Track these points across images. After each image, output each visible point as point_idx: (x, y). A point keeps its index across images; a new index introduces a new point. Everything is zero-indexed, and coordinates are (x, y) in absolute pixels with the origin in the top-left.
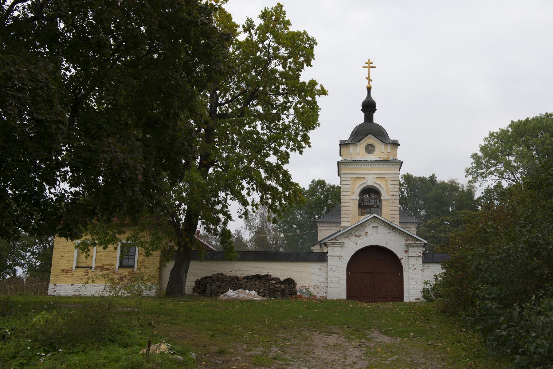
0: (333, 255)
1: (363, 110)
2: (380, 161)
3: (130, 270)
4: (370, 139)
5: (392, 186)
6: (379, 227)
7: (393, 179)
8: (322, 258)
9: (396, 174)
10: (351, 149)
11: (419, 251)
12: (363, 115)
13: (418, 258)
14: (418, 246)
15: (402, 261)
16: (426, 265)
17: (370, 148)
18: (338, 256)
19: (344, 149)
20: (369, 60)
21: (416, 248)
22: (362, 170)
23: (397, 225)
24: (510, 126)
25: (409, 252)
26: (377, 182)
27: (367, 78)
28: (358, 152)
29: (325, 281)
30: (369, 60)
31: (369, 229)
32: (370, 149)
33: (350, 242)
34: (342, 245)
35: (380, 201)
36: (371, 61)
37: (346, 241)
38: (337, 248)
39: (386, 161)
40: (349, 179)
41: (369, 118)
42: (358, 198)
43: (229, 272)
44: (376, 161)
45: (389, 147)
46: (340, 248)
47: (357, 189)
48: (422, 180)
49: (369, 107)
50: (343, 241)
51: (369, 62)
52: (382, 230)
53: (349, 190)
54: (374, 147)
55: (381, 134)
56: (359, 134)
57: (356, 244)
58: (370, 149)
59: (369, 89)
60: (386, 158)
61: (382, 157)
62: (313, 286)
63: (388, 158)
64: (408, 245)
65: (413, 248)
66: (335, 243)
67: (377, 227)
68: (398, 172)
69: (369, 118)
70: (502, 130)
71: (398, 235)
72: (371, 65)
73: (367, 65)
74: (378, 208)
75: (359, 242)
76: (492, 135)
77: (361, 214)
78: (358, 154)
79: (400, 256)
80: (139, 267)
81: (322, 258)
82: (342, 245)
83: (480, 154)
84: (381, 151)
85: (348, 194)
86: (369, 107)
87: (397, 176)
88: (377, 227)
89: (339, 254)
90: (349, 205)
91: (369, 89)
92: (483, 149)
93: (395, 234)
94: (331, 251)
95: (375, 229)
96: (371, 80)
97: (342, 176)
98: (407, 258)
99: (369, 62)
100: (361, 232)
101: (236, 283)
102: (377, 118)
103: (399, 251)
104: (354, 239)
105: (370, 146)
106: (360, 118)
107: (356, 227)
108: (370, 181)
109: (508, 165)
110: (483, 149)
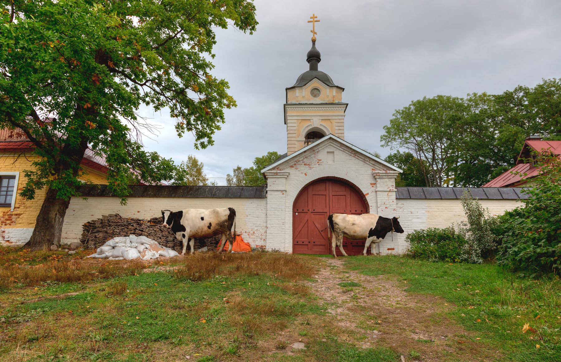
0: (275, 189)
1: (309, 60)
2: (326, 104)
3: (5, 210)
4: (315, 83)
5: (337, 128)
6: (337, 152)
7: (338, 121)
9: (341, 116)
11: (390, 184)
12: (308, 65)
13: (390, 194)
14: (389, 177)
15: (368, 198)
16: (401, 202)
18: (282, 191)
19: (290, 93)
20: (314, 15)
21: (387, 180)
22: (307, 112)
25: (378, 185)
26: (321, 123)
27: (311, 31)
28: (303, 95)
29: (265, 225)
30: (314, 15)
33: (297, 172)
36: (315, 16)
37: (292, 171)
38: (280, 179)
40: (295, 121)
41: (314, 67)
42: (304, 139)
43: (136, 213)
46: (283, 180)
47: (303, 131)
49: (314, 58)
50: (287, 170)
51: (314, 17)
52: (341, 156)
53: (296, 132)
54: (319, 91)
55: (326, 80)
56: (303, 81)
57: (306, 174)
58: (315, 92)
59: (314, 41)
60: (332, 102)
62: (247, 231)
63: (333, 101)
65: (382, 180)
66: (277, 173)
67: (333, 152)
68: (343, 114)
69: (314, 67)
71: (362, 163)
72: (315, 19)
73: (312, 20)
75: (309, 172)
78: (303, 97)
79: (364, 191)
80: (17, 206)
82: (287, 176)
85: (294, 135)
86: (314, 58)
87: (343, 118)
88: (333, 152)
89: (283, 188)
90: (296, 146)
91: (314, 41)
93: (357, 161)
95: (331, 156)
96: (316, 33)
97: (289, 125)
98: (374, 193)
99: (314, 17)
101: (134, 227)
102: (321, 67)
105: (316, 90)
106: (306, 67)
107: (305, 152)
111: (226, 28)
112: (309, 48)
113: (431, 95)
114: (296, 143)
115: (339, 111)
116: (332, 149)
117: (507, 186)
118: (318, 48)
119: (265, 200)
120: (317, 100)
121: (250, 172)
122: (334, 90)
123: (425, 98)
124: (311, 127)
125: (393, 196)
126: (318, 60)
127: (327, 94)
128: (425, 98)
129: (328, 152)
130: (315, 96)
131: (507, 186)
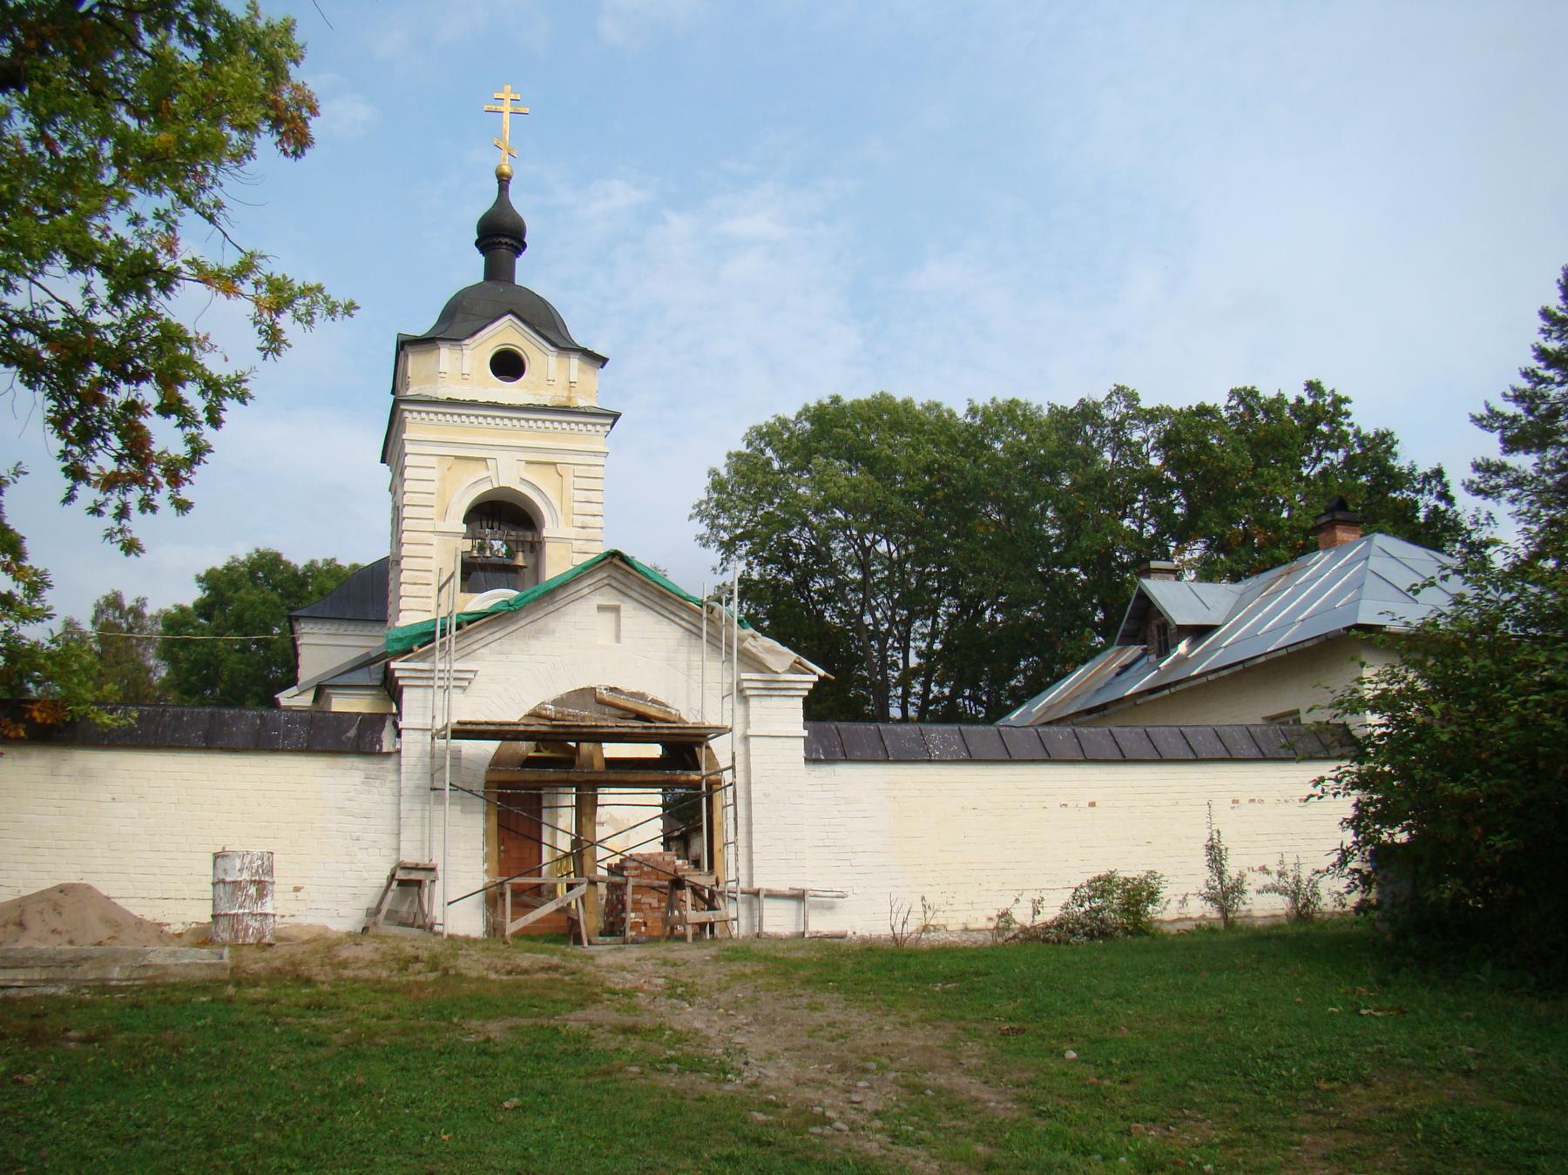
2: (544, 409)
4: (505, 333)
5: (581, 496)
6: (628, 609)
12: (479, 260)
19: (416, 363)
38: (483, 719)
40: (433, 461)
42: (463, 528)
49: (500, 236)
53: (433, 500)
55: (544, 322)
56: (459, 320)
58: (508, 365)
59: (503, 180)
63: (569, 399)
86: (500, 236)
87: (600, 461)
91: (503, 180)
102: (528, 272)
106: (471, 268)
112: (484, 202)
113: (856, 390)
114: (434, 539)
115: (591, 438)
117: (1049, 723)
118: (520, 202)
119: (389, 764)
122: (575, 361)
124: (485, 487)
126: (519, 246)
127: (549, 371)
129: (601, 608)
131: (1049, 723)
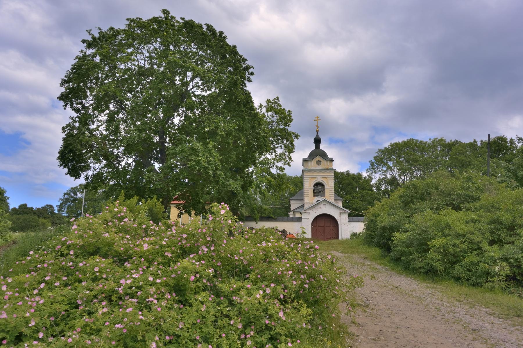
4: (318, 158)
8: (299, 220)
10: (309, 163)
11: (346, 216)
14: (345, 214)
16: (350, 223)
17: (319, 162)
19: (305, 163)
22: (314, 174)
23: (333, 201)
24: (389, 225)
28: (312, 165)
31: (322, 205)
32: (319, 163)
34: (309, 213)
35: (324, 190)
39: (327, 169)
41: (317, 147)
44: (322, 170)
45: (329, 162)
48: (342, 173)
51: (317, 118)
55: (324, 155)
56: (312, 156)
58: (319, 163)
59: (317, 132)
61: (324, 168)
64: (341, 214)
69: (317, 147)
70: (385, 148)
74: (323, 195)
76: (380, 150)
77: (314, 196)
81: (299, 220)
83: (374, 161)
84: (324, 164)
91: (317, 132)
92: (375, 158)
94: (304, 217)
99: (317, 118)
100: (318, 207)
102: (322, 147)
103: (337, 217)
104: (314, 210)
106: (313, 147)
108: (319, 180)
109: (389, 168)
110: (375, 158)
111: (261, 104)
116: (325, 203)
120: (320, 167)
121: (52, 213)
123: (451, 141)
125: (347, 220)
128: (451, 141)
130: (318, 165)
